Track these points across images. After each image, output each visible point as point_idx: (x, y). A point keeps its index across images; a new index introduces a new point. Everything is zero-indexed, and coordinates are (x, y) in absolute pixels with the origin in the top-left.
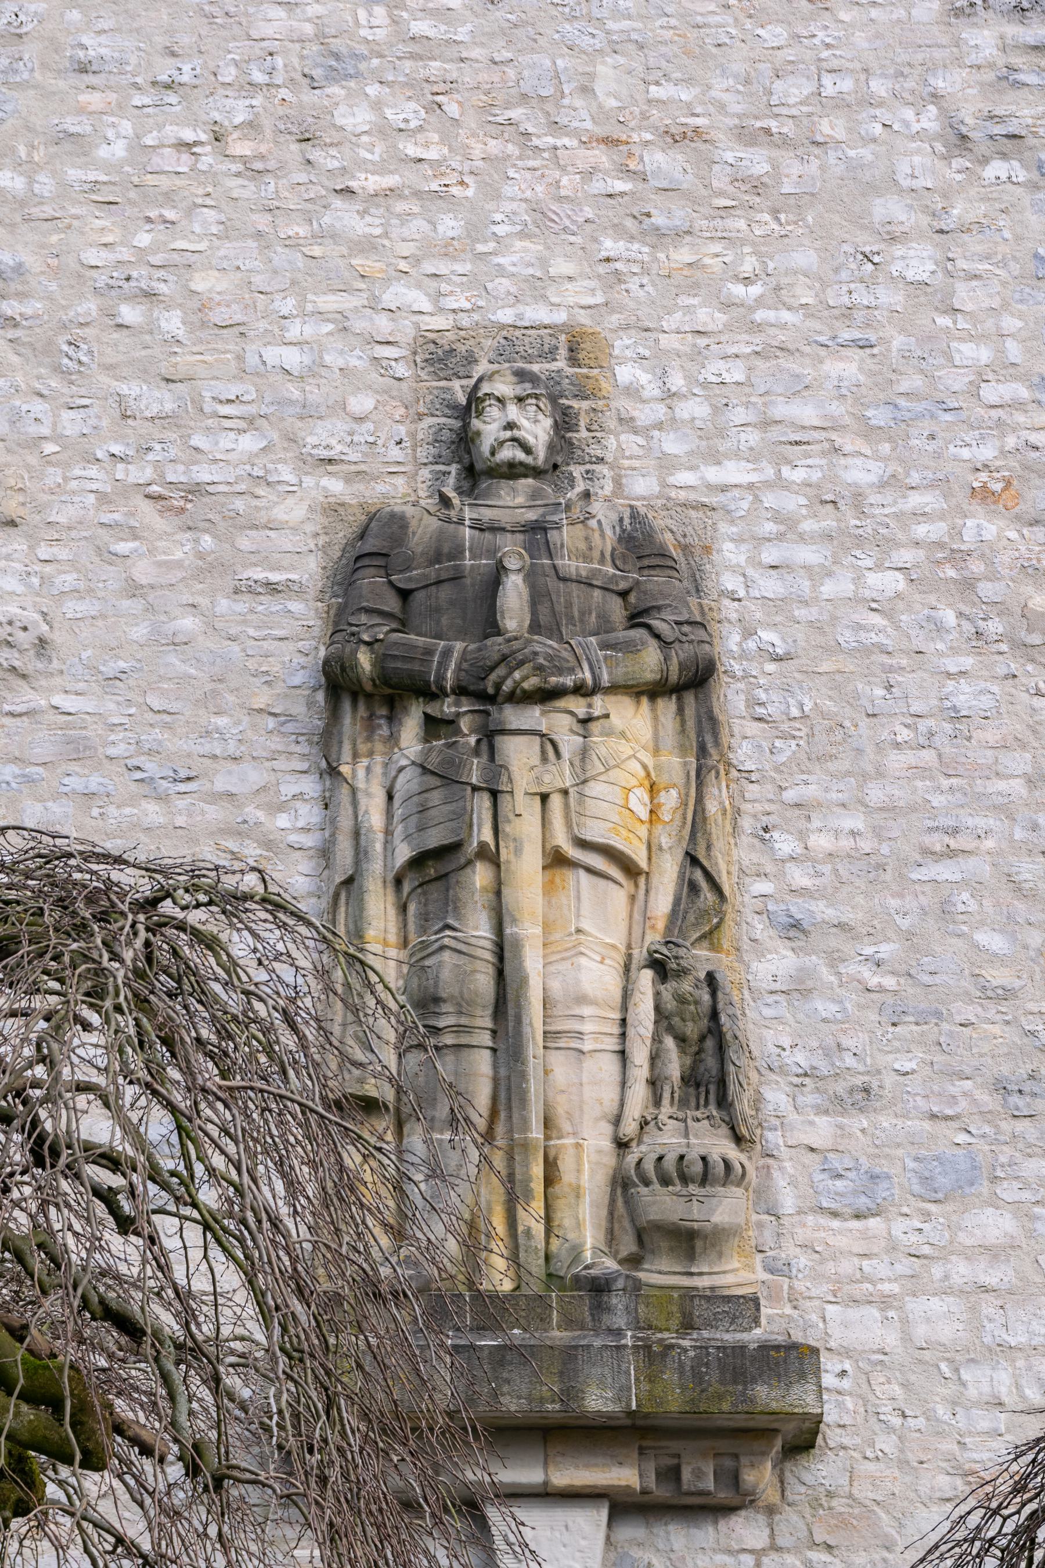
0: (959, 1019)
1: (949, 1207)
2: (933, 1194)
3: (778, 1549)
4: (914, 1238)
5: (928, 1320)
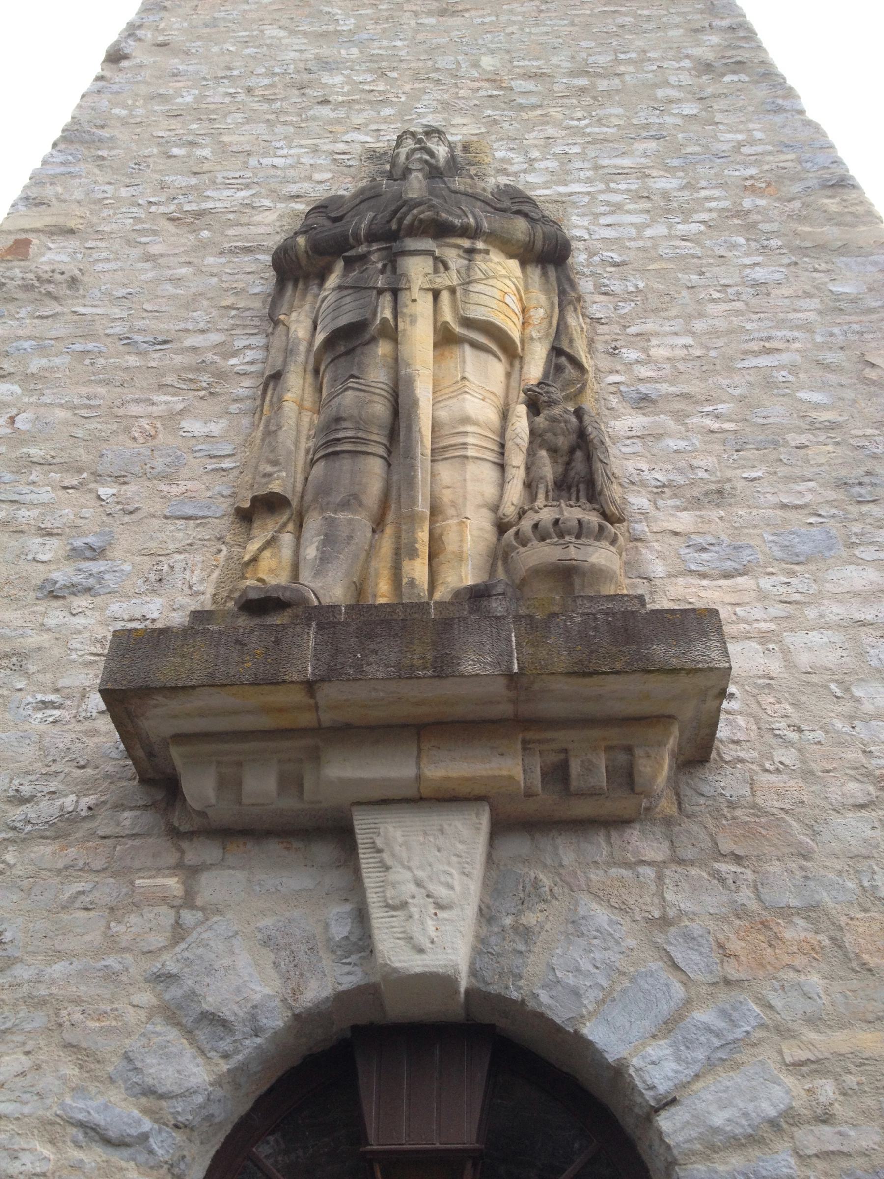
0: (793, 444)
1: (812, 567)
2: (794, 560)
3: (681, 862)
4: (783, 589)
5: (810, 649)
